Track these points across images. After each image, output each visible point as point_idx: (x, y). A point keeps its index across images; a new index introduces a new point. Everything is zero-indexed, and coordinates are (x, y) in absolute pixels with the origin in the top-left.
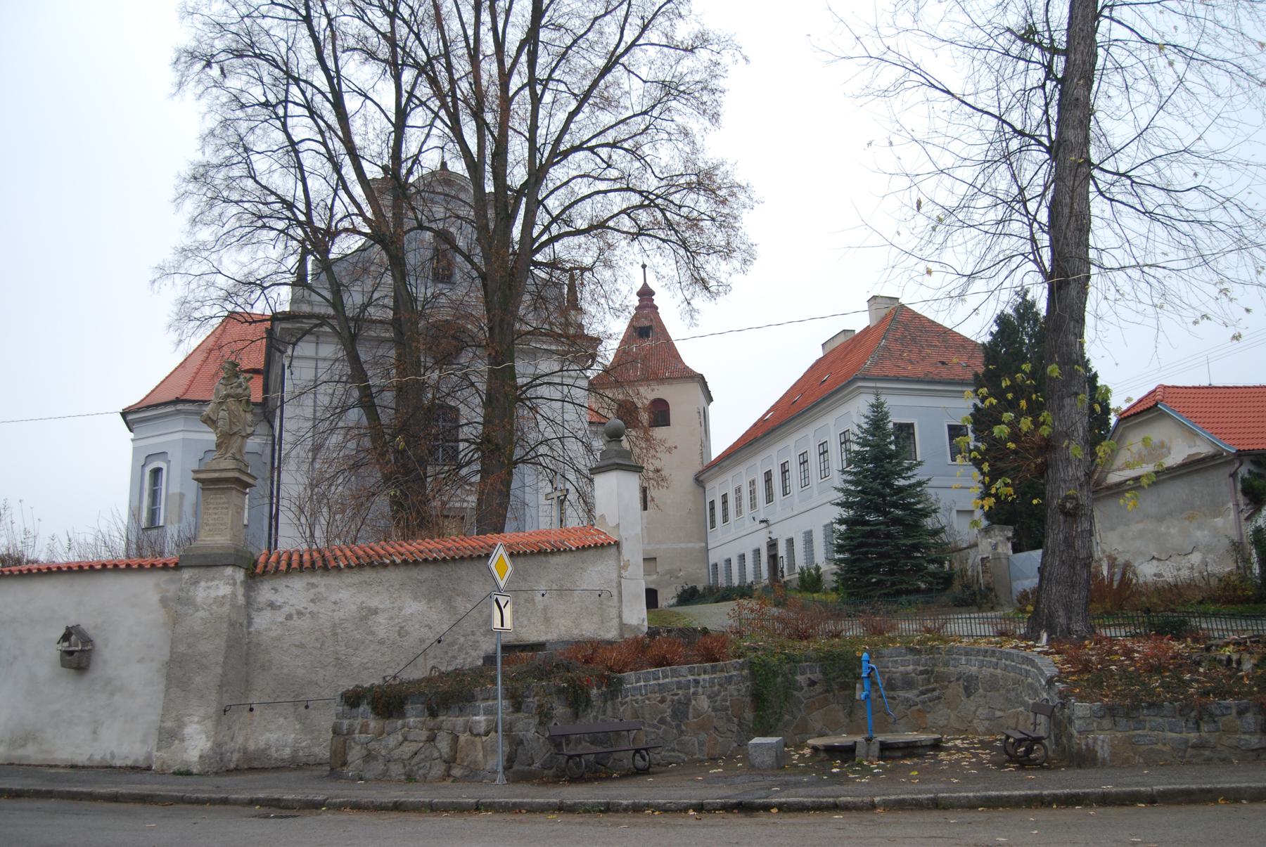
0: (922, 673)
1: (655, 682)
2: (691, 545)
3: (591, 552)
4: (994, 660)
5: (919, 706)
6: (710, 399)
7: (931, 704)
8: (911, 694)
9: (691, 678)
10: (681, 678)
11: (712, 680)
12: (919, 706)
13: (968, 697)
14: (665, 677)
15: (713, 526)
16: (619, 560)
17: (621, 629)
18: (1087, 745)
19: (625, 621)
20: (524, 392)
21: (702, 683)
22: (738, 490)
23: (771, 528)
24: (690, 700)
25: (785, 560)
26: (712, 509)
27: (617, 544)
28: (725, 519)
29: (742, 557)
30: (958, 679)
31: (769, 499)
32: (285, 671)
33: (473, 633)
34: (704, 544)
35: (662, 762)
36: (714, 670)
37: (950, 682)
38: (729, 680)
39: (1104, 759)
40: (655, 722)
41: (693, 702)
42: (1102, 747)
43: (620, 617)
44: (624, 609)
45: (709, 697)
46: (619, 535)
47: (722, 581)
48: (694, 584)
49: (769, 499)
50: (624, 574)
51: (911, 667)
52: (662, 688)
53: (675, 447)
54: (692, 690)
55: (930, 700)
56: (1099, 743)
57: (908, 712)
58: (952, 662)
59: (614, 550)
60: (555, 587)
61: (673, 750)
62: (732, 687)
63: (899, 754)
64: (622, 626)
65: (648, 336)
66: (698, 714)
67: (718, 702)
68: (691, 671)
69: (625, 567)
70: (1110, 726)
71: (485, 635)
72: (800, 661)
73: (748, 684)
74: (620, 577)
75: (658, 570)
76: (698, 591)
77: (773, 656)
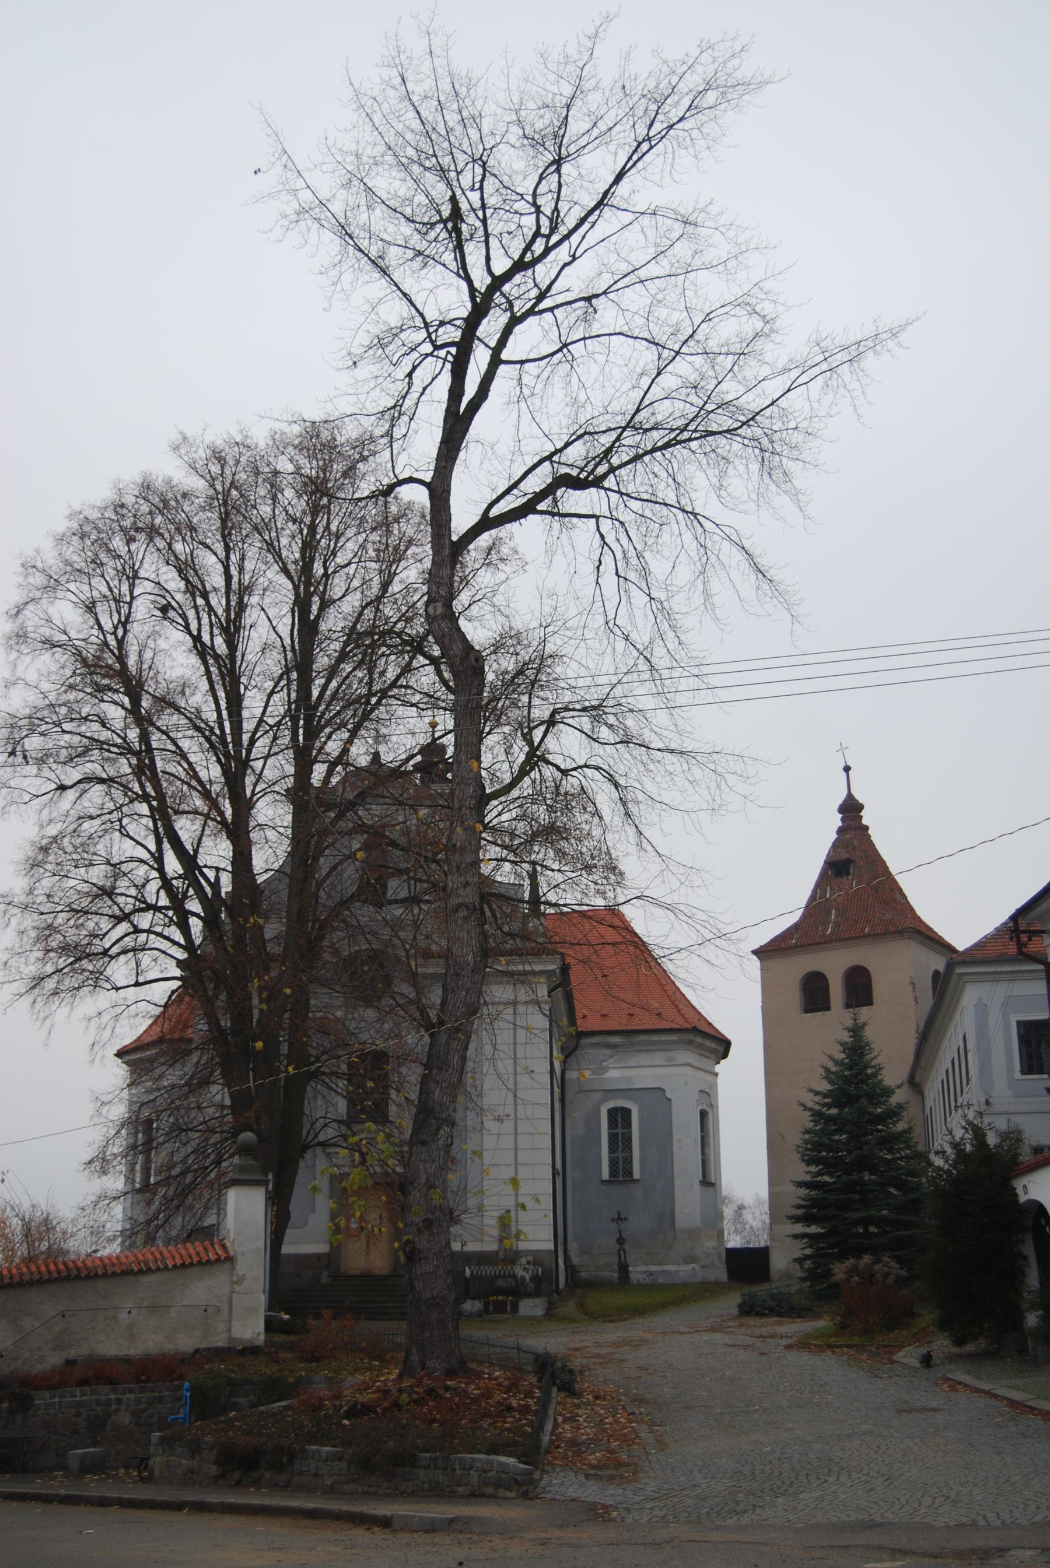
9: (113, 1396)
10: (102, 1397)
11: (138, 1401)
14: (83, 1394)
16: (232, 1275)
32: (908, 1356)
33: (40, 1348)
36: (142, 1390)
41: (114, 1418)
43: (229, 1331)
44: (234, 1323)
54: (114, 1407)
59: (227, 1266)
60: (145, 1304)
65: (848, 874)
69: (240, 1281)
71: (54, 1350)
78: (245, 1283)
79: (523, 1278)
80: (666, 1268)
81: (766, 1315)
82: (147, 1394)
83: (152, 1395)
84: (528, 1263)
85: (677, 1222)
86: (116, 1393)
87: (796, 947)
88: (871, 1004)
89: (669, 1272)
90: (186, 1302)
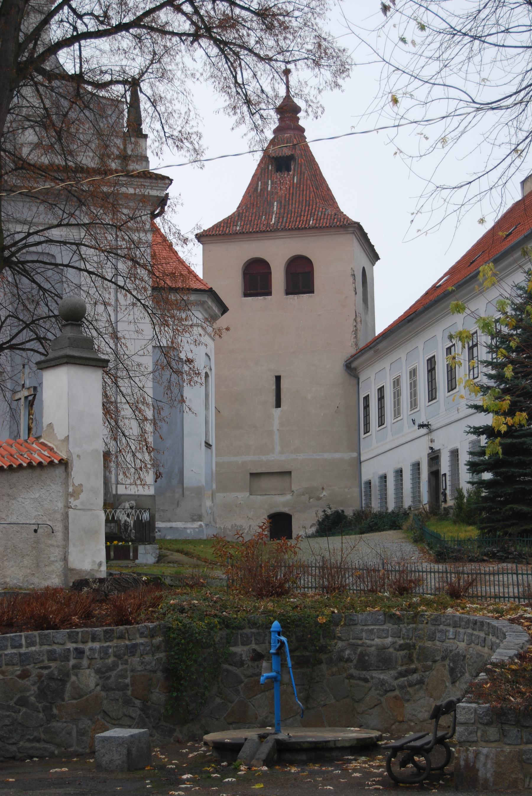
0: (402, 647)
1: (14, 651)
2: (337, 455)
3: (24, 474)
4: (482, 635)
5: (397, 692)
6: (374, 257)
7: (410, 690)
8: (386, 676)
9: (71, 646)
10: (55, 647)
11: (104, 651)
12: (397, 692)
13: (453, 683)
15: (367, 431)
16: (66, 484)
17: (66, 576)
18: (466, 760)
19: (71, 565)
20: (13, 254)
21: (87, 653)
22: (397, 382)
23: (434, 435)
24: (68, 675)
25: (448, 478)
26: (367, 407)
27: (64, 464)
28: (381, 422)
29: (399, 473)
30: (444, 659)
31: (432, 396)
34: (355, 455)
35: (19, 755)
37: (435, 661)
38: (132, 650)
39: (486, 780)
40: (12, 703)
41: (73, 678)
42: (485, 765)
43: (65, 559)
45: (98, 672)
46: (68, 451)
47: (376, 506)
48: (340, 509)
49: (432, 396)
50: (73, 502)
51: (390, 640)
52: (24, 659)
53: (228, 329)
54: (72, 662)
55: (411, 685)
56: (482, 758)
57: (383, 699)
58: (438, 635)
59: (60, 471)
61: (38, 740)
62: (136, 660)
63: (304, 757)
64: (67, 571)
65: (289, 170)
66: (78, 694)
67: (112, 679)
68: (72, 638)
69: (76, 494)
70: (497, 737)
72: (242, 628)
73: (162, 655)
74: (68, 506)
75: (293, 488)
76: (345, 517)
77: (201, 620)
78: (82, 496)
79: (126, 524)
80: (174, 525)
81: (484, 561)
82: (115, 642)
83: (122, 643)
84: (131, 508)
85: (185, 481)
86: (76, 642)
87: (242, 233)
88: (313, 292)
89: (177, 529)
90: (13, 519)
